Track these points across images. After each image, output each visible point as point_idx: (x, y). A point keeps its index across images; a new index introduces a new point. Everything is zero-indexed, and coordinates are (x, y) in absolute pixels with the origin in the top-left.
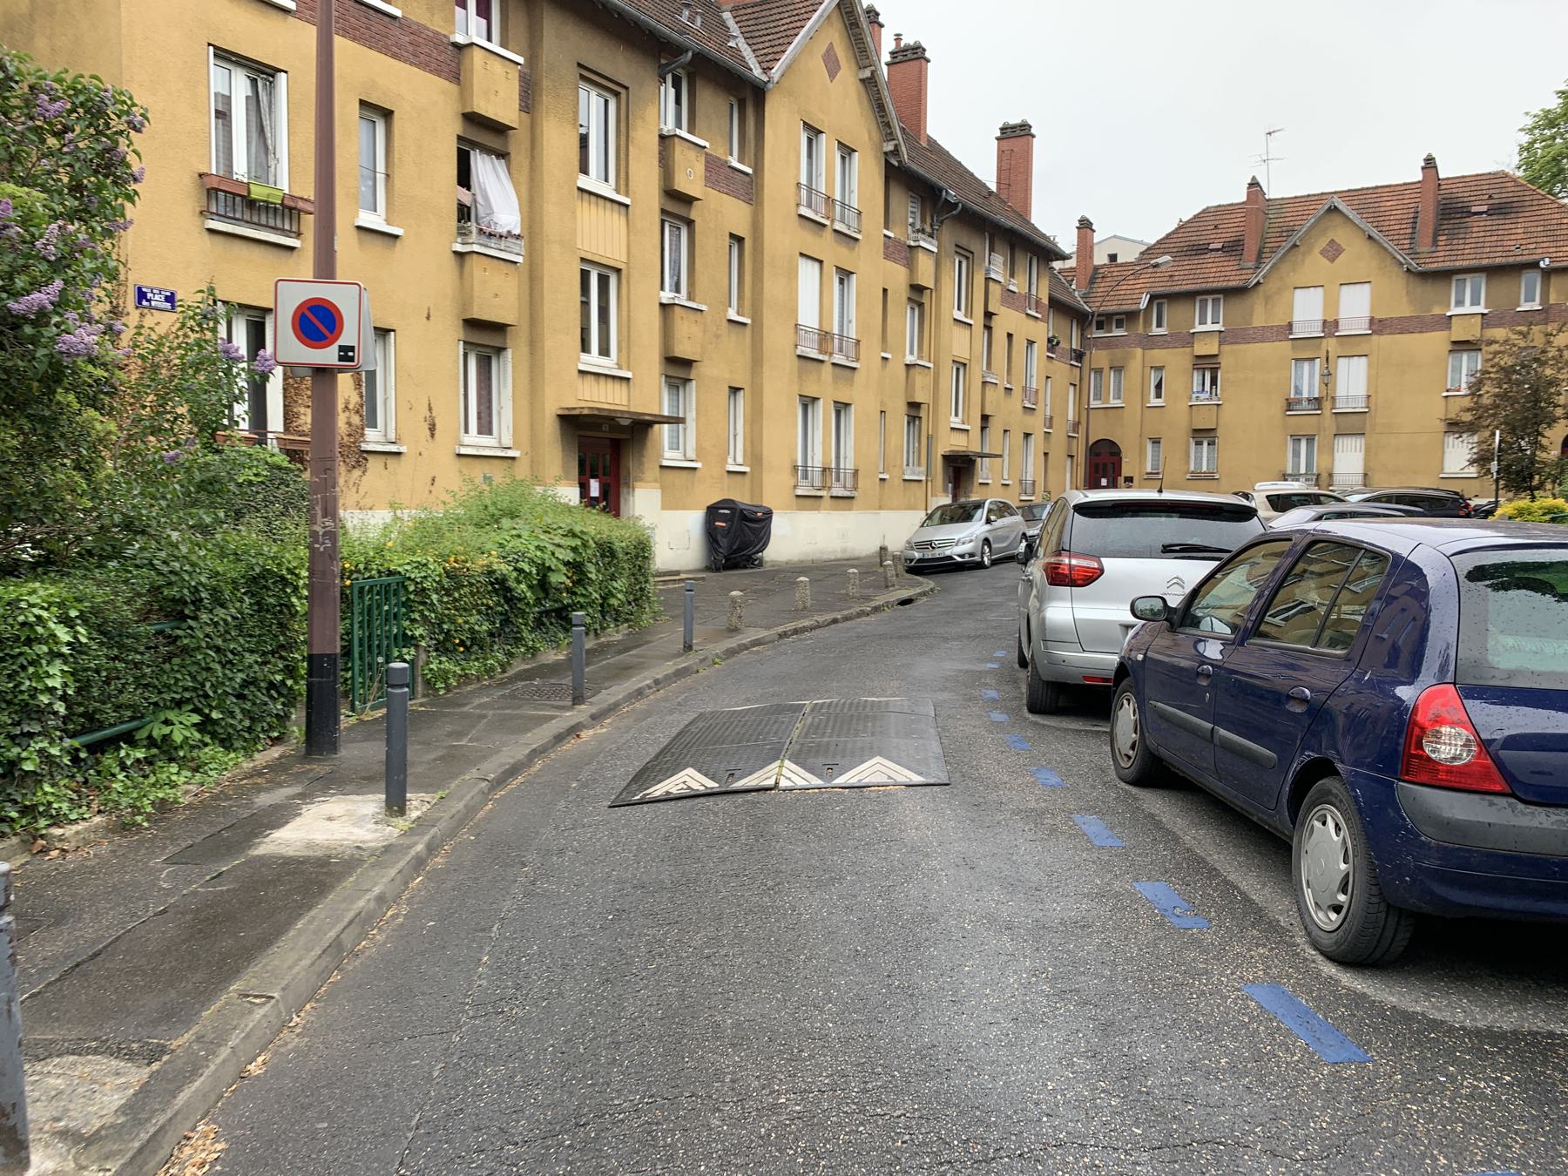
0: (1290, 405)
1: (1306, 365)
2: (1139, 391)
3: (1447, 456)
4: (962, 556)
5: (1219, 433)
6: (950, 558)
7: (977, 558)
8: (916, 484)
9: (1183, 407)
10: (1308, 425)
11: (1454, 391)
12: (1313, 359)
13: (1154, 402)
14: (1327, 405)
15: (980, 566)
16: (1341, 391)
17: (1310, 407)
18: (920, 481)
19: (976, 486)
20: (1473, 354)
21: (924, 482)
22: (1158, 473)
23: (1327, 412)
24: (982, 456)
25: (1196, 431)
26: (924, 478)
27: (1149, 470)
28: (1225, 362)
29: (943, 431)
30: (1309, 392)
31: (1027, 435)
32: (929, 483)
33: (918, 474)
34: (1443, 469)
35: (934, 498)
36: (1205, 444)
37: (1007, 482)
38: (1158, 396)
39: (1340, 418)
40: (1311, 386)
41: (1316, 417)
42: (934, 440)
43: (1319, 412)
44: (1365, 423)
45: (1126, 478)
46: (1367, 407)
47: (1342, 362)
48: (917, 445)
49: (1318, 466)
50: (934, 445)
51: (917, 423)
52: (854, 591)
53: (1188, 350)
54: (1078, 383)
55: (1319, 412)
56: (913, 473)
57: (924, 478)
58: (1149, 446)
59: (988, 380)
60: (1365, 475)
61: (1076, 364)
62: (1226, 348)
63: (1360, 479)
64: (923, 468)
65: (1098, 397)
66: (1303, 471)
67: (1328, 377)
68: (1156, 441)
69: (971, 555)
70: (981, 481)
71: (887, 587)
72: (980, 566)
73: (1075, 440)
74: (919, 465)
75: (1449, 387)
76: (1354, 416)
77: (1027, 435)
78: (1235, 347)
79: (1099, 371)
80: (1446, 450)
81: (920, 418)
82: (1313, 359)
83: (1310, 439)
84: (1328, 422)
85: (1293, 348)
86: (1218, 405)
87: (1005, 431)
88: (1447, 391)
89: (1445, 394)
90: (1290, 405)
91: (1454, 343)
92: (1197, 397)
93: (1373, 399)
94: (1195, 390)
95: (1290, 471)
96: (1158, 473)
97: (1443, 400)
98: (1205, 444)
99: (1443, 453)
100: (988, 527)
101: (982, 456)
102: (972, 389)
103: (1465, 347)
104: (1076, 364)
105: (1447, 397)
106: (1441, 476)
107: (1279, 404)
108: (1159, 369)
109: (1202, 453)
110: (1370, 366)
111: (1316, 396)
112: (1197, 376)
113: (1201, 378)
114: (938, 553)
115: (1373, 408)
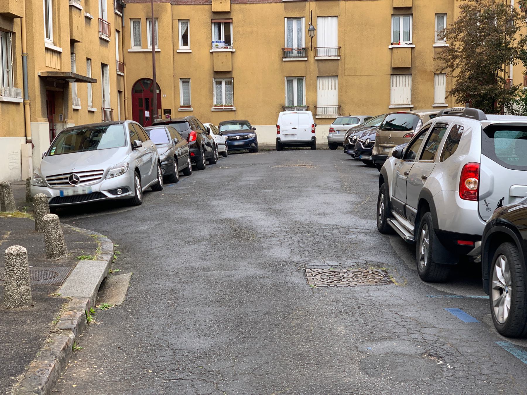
0: (285, 53)
1: (295, 23)
2: (171, 39)
3: (393, 92)
4: (113, 191)
5: (234, 75)
6: (98, 194)
7: (130, 193)
8: (13, 107)
9: (205, 52)
10: (298, 69)
11: (396, 44)
12: (299, 18)
13: (182, 49)
14: (311, 54)
15: (132, 202)
16: (320, 43)
17: (300, 55)
18: (18, 104)
19: (70, 113)
20: (407, 18)
21: (22, 105)
22: (189, 107)
23: (311, 60)
24: (79, 79)
25: (216, 73)
26: (21, 101)
27: (182, 104)
28: (236, 17)
29: (39, 52)
30: (298, 45)
31: (104, 65)
32: (28, 107)
33: (16, 96)
34: (390, 101)
35: (34, 124)
36: (224, 83)
37: (92, 109)
38: (185, 42)
39: (321, 64)
40: (299, 39)
41: (304, 63)
42: (30, 57)
43: (306, 59)
44: (338, 69)
45: (165, 110)
46: (339, 56)
47: (320, 21)
48: (12, 63)
49: (307, 100)
50: (30, 69)
51: (11, 39)
52: (23, 289)
53: (207, 7)
54: (121, 30)
55: (306, 59)
56: (9, 94)
57: (21, 101)
58: (181, 84)
59: (74, 4)
60: (340, 107)
61: (119, 13)
62: (236, 7)
63: (335, 110)
64: (20, 90)
65: (137, 42)
66: (295, 104)
67: (312, 31)
68: (186, 81)
69: (125, 189)
70: (74, 107)
71: (51, 256)
72: (132, 202)
73: (122, 79)
74: (16, 85)
75: (392, 42)
76: (330, 63)
77: (104, 65)
78: (243, 6)
79: (137, 21)
80: (393, 88)
81: (14, 33)
82: (299, 18)
83: (300, 80)
84: (313, 67)
85: (285, 8)
86: (232, 52)
87: (88, 59)
88: (392, 44)
89: (390, 47)
90: (285, 53)
91: (395, 8)
92: (216, 46)
93: (342, 49)
94: (213, 40)
95: (287, 105)
96: (189, 107)
97: (389, 51)
98: (224, 83)
99: (390, 90)
100: (136, 154)
101: (79, 79)
102: (61, 8)
103: (402, 12)
104: (119, 13)
105: (392, 49)
106: (390, 107)
107: (276, 54)
108: (184, 22)
109: (221, 90)
110: (339, 24)
111: (304, 47)
112: (214, 30)
113: (217, 31)
114: (81, 189)
115: (343, 56)
